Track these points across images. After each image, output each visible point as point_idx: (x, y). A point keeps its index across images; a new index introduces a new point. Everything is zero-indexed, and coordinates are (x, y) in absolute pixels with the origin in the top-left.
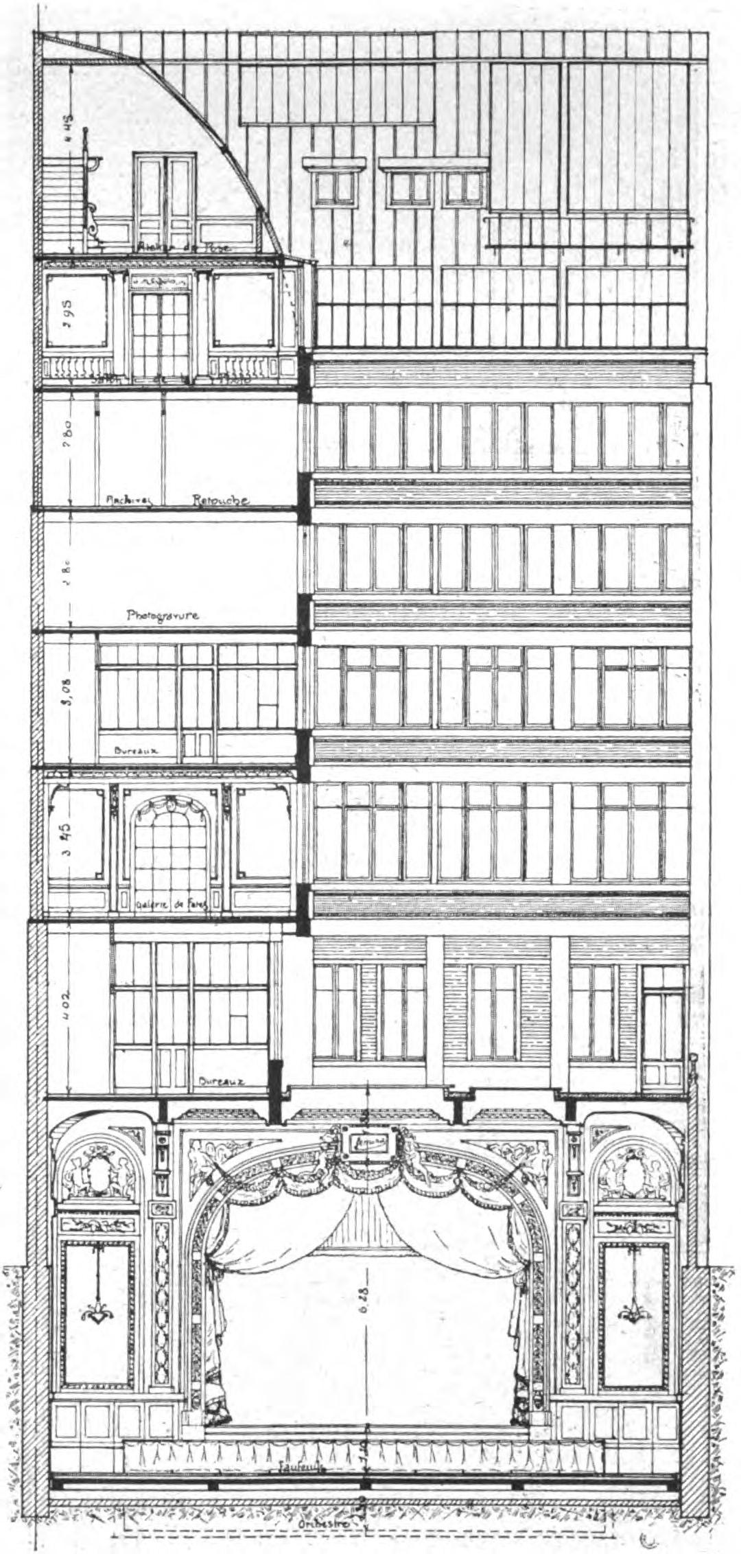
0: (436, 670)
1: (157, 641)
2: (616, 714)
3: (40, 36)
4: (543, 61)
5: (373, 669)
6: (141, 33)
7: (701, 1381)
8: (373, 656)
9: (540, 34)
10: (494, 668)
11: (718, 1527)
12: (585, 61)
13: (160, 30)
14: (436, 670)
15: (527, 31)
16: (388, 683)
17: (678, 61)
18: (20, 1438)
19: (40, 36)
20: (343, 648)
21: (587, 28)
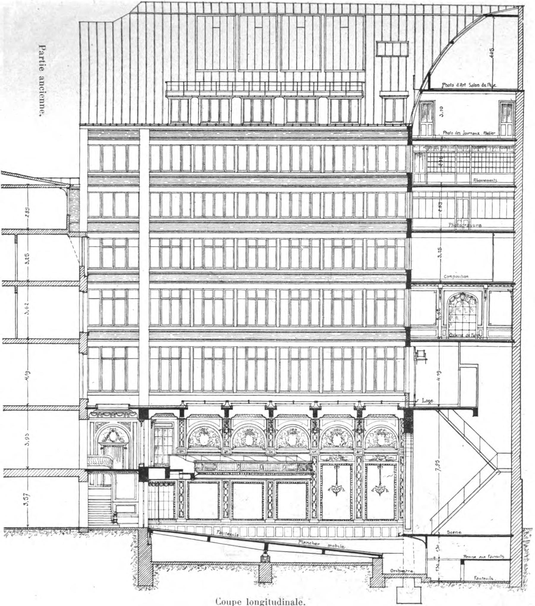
0: (235, 247)
1: (375, 237)
2: (208, 263)
3: (523, 6)
4: (356, 15)
5: (257, 247)
6: (399, 5)
7: (515, 529)
8: (257, 242)
9: (448, 6)
10: (386, 247)
11: (135, 591)
12: (204, 14)
13: (349, 2)
14: (235, 247)
15: (222, 3)
16: (120, 252)
17: (360, 15)
18: (523, 558)
19: (523, 6)
20: (375, 239)
21: (408, 3)
